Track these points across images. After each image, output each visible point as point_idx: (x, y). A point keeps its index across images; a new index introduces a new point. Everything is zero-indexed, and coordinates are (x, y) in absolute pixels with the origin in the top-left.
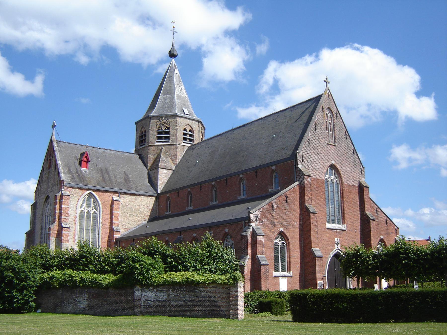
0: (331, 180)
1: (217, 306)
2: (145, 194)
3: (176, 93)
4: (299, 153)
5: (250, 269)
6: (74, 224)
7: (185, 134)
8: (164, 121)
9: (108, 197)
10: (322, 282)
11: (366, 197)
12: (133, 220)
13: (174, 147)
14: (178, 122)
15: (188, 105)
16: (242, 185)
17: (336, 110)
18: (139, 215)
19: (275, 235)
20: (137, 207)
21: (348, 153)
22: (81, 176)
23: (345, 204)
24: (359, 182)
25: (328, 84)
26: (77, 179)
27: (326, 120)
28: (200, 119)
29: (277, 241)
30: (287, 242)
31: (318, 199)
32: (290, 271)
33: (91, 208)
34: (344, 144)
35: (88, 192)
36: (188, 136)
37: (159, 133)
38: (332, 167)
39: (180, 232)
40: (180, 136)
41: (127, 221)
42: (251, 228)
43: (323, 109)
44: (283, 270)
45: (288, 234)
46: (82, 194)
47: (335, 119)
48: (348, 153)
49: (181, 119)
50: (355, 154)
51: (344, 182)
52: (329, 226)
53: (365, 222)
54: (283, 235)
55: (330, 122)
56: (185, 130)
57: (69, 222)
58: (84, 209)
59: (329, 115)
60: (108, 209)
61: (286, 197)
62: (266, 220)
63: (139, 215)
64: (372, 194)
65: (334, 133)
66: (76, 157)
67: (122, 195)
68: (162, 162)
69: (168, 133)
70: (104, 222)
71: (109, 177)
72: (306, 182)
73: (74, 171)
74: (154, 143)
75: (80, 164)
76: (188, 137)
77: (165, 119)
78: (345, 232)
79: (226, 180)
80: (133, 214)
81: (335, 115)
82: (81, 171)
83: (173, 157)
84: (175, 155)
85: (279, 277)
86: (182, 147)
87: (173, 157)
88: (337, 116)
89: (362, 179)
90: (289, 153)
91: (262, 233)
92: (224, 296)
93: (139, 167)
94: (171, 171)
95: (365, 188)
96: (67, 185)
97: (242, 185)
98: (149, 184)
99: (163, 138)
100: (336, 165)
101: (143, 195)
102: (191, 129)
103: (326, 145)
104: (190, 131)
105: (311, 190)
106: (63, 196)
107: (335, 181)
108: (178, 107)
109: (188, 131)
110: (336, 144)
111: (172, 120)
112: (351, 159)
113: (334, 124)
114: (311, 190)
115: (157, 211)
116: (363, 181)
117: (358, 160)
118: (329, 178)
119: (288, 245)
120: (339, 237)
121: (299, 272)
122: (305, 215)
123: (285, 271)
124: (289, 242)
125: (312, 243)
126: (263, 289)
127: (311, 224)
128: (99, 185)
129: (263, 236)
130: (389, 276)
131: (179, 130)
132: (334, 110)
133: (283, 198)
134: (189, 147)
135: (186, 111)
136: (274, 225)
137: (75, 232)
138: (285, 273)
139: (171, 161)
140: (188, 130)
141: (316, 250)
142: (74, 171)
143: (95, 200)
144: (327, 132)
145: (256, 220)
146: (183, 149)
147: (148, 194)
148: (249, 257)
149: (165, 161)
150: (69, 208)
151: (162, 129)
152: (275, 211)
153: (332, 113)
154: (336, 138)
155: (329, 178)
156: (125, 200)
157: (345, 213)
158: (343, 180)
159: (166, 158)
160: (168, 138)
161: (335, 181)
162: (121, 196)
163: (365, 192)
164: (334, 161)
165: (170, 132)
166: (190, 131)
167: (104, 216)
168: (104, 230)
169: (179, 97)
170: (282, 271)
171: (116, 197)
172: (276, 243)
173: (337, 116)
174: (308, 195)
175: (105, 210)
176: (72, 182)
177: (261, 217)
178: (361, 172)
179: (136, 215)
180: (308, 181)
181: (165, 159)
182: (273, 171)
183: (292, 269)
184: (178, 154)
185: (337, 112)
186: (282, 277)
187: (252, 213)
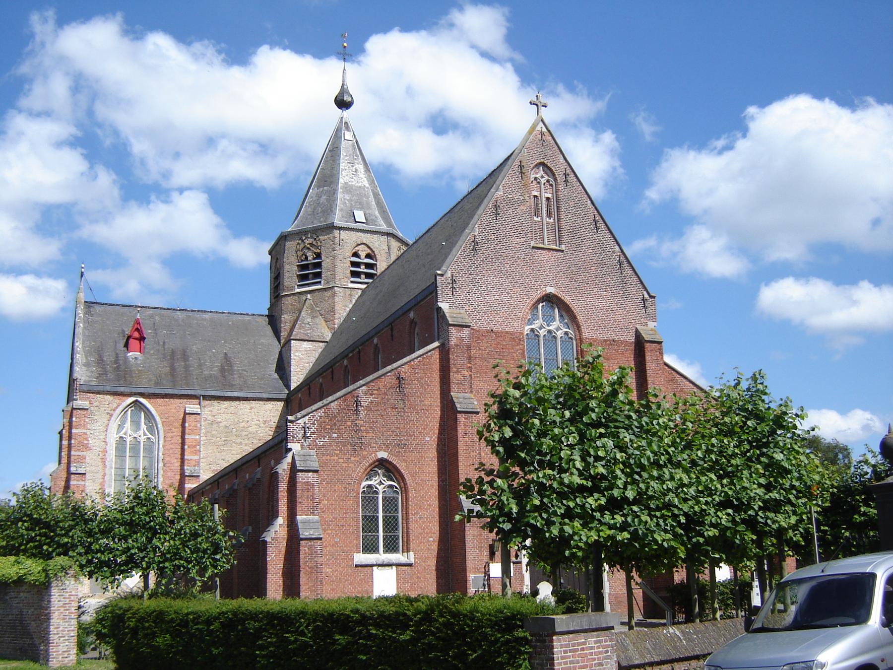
0: (550, 332)
2: (259, 395)
3: (341, 180)
4: (442, 275)
5: (284, 550)
6: (101, 466)
7: (354, 264)
8: (311, 240)
9: (176, 407)
12: (233, 452)
13: (328, 294)
14: (337, 240)
15: (368, 204)
19: (361, 469)
21: (602, 264)
22: (123, 367)
24: (637, 331)
26: (111, 376)
27: (537, 194)
30: (402, 484)
32: (408, 551)
33: (141, 432)
35: (132, 399)
36: (363, 267)
37: (303, 267)
38: (551, 300)
40: (343, 268)
42: (290, 455)
44: (391, 547)
46: (119, 405)
47: (561, 187)
48: (602, 264)
49: (344, 234)
51: (586, 334)
54: (390, 467)
55: (550, 196)
56: (356, 255)
57: (88, 460)
58: (125, 434)
59: (543, 181)
60: (178, 432)
63: (246, 442)
66: (123, 331)
67: (207, 402)
68: (301, 327)
69: (319, 265)
70: (167, 459)
71: (187, 367)
73: (109, 358)
74: (293, 288)
75: (126, 345)
76: (362, 269)
77: (312, 237)
79: (359, 352)
80: (233, 439)
81: (560, 178)
82: (126, 359)
84: (332, 311)
85: (372, 566)
87: (329, 315)
88: (566, 181)
91: (315, 465)
93: (263, 341)
94: (321, 344)
95: (647, 345)
96: (85, 388)
98: (276, 376)
99: (311, 276)
101: (254, 399)
102: (369, 251)
103: (529, 250)
104: (368, 256)
105: (470, 358)
106: (75, 412)
107: (559, 334)
108: (341, 210)
110: (563, 247)
111: (326, 237)
114: (470, 358)
116: (649, 329)
117: (635, 279)
118: (541, 327)
119: (405, 490)
121: (435, 553)
123: (375, 550)
124: (405, 484)
127: (460, 439)
128: (158, 384)
129: (316, 471)
130: (617, 559)
132: (559, 168)
133: (390, 380)
134: (363, 291)
135: (360, 216)
136: (358, 446)
137: (104, 481)
138: (382, 556)
139: (324, 323)
140: (363, 254)
142: (109, 358)
143: (149, 416)
144: (539, 219)
145: (305, 437)
146: (351, 295)
147: (265, 396)
148: (281, 521)
150: (86, 434)
151: (306, 258)
152: (363, 413)
153: (554, 175)
154: (564, 233)
155: (541, 327)
156: (212, 411)
158: (584, 329)
159: (314, 317)
160: (318, 275)
161: (559, 334)
162: (204, 403)
164: (556, 286)
166: (368, 256)
167: (168, 446)
168: (169, 474)
169: (348, 189)
170: (386, 552)
171: (192, 407)
172: (370, 486)
173: (566, 181)
175: (170, 435)
176: (99, 382)
178: (645, 307)
179: (239, 440)
180: (462, 339)
181: (309, 320)
183: (412, 545)
184: (337, 308)
185: (569, 171)
186: (379, 565)
187: (292, 422)
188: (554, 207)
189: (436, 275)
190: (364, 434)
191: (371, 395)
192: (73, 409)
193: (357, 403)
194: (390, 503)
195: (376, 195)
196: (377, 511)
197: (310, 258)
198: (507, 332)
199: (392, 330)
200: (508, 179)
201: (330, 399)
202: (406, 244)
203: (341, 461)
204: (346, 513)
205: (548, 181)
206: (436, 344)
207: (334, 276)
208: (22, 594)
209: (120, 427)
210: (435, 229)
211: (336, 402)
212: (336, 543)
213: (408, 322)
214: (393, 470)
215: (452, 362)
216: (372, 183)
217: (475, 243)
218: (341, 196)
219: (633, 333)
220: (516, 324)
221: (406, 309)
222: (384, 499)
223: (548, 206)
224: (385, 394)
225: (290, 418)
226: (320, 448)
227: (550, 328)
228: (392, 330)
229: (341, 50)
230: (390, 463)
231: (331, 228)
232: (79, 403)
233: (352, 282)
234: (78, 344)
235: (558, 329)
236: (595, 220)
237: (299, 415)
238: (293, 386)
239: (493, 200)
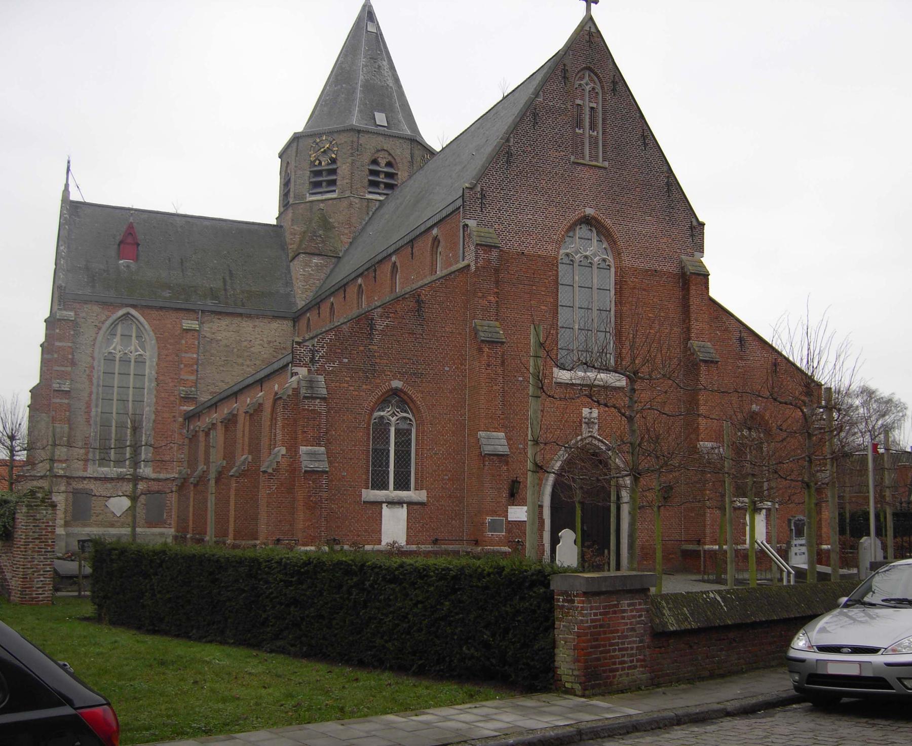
7: (373, 173)
11: (694, 301)
12: (234, 373)
18: (248, 362)
20: (245, 343)
36: (382, 176)
38: (587, 221)
46: (108, 317)
54: (405, 397)
56: (375, 162)
58: (115, 349)
59: (588, 88)
61: (419, 302)
63: (248, 362)
69: (333, 172)
70: (161, 378)
76: (381, 178)
85: (381, 503)
99: (324, 184)
104: (389, 164)
118: (577, 252)
123: (408, 488)
126: (526, 519)
137: (90, 400)
138: (392, 493)
140: (383, 162)
151: (320, 163)
152: (377, 338)
160: (333, 183)
164: (596, 207)
165: (338, 171)
166: (389, 164)
168: (163, 395)
170: (416, 489)
172: (382, 417)
182: (436, 240)
190: (378, 361)
191: (388, 318)
193: (372, 327)
197: (323, 163)
198: (539, 256)
203: (352, 388)
204: (355, 446)
212: (343, 477)
214: (409, 401)
220: (550, 248)
226: (329, 373)
230: (405, 393)
233: (370, 192)
235: (595, 255)
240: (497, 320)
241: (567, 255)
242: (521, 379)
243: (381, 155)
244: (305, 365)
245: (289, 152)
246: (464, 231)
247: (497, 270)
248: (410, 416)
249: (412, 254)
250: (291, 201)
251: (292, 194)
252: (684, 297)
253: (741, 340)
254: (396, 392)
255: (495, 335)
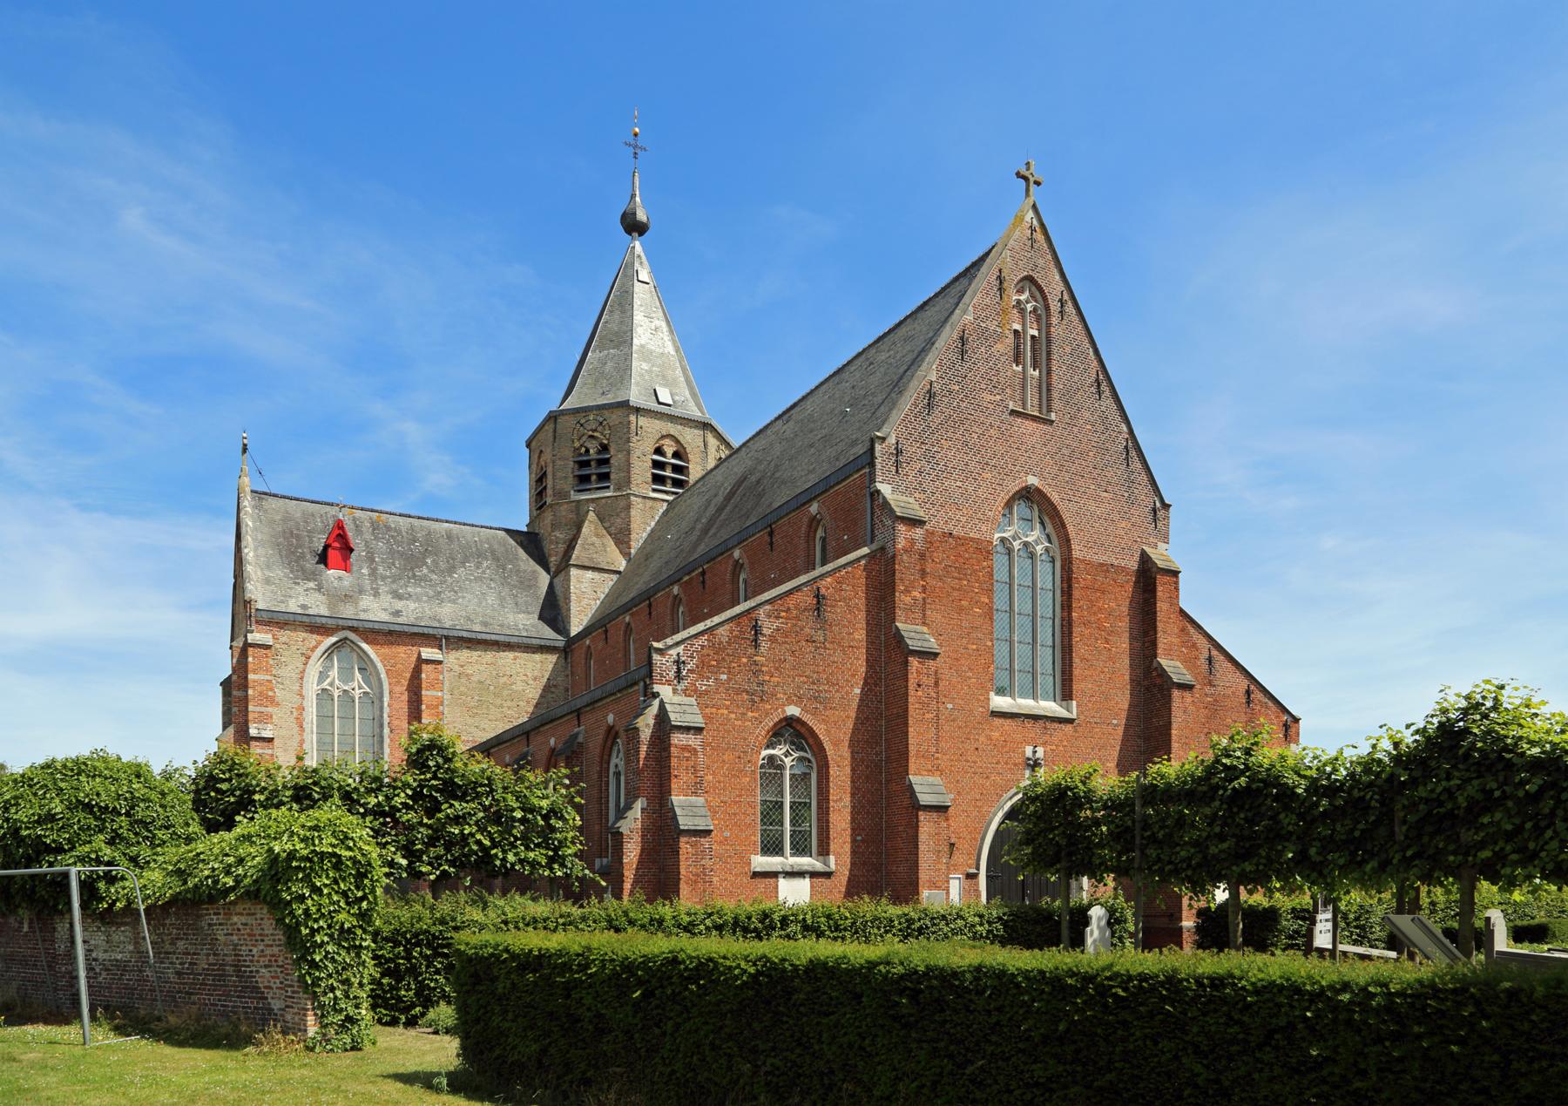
0: (1026, 544)
1: (256, 989)
7: (656, 464)
10: (954, 887)
11: (1162, 606)
14: (633, 427)
15: (675, 380)
16: (742, 586)
17: (1061, 287)
20: (502, 680)
23: (1076, 630)
24: (1144, 554)
25: (1033, 187)
27: (1017, 327)
28: (708, 417)
29: (778, 751)
31: (961, 610)
34: (1087, 415)
36: (669, 469)
38: (1028, 495)
39: (527, 734)
40: (641, 470)
41: (470, 721)
42: (656, 702)
43: (1000, 279)
44: (800, 849)
45: (819, 729)
46: (319, 643)
47: (1055, 320)
49: (643, 421)
50: (1133, 453)
51: (1076, 554)
52: (1000, 702)
53: (1152, 694)
54: (803, 730)
55: (1036, 333)
56: (659, 451)
58: (331, 684)
59: (1029, 307)
62: (724, 677)
64: (1193, 596)
65: (1049, 372)
69: (606, 462)
72: (901, 543)
76: (668, 473)
78: (1068, 728)
79: (703, 573)
81: (1055, 306)
83: (622, 539)
86: (650, 503)
89: (1156, 547)
90: (860, 449)
91: (698, 721)
92: (276, 950)
96: (265, 616)
97: (742, 586)
100: (1046, 490)
103: (1006, 416)
104: (676, 455)
106: (250, 650)
109: (669, 454)
110: (1053, 416)
112: (1116, 472)
113: (1049, 342)
115: (567, 690)
116: (1162, 554)
120: (1044, 744)
122: (889, 657)
125: (912, 760)
127: (911, 692)
131: (638, 453)
132: (1054, 288)
133: (805, 598)
138: (805, 862)
140: (669, 451)
141: (926, 786)
144: (1020, 368)
149: (594, 540)
151: (587, 451)
152: (764, 645)
153: (1045, 298)
154: (1055, 394)
157: (1076, 660)
160: (605, 477)
161: (1039, 549)
163: (1159, 588)
169: (647, 355)
171: (428, 653)
172: (771, 758)
174: (907, 591)
177: (703, 664)
179: (499, 702)
180: (912, 542)
182: (814, 522)
183: (832, 847)
185: (1066, 297)
188: (1042, 351)
189: (872, 442)
191: (777, 618)
192: (246, 645)
193: (757, 629)
194: (800, 780)
195: (684, 370)
196: (781, 793)
198: (972, 539)
199: (771, 534)
200: (980, 293)
201: (716, 619)
202: (728, 445)
205: (1035, 309)
206: (865, 550)
207: (628, 482)
208: (235, 919)
209: (323, 676)
210: (816, 398)
211: (727, 627)
213: (805, 520)
214: (807, 734)
215: (898, 575)
216: (677, 351)
217: (931, 394)
218: (638, 365)
219: (1137, 557)
220: (984, 528)
221: (803, 499)
222: (793, 776)
223: (1034, 350)
224: (797, 618)
225: (656, 645)
227: (1029, 539)
228: (771, 534)
229: (631, 139)
230: (804, 724)
231: (625, 405)
232: (256, 636)
233: (654, 490)
234: (249, 553)
235: (1037, 542)
236: (1097, 380)
237: (669, 641)
238: (574, 631)
239: (959, 327)
240: (924, 624)
241: (1003, 540)
242: (950, 706)
243: (667, 442)
244: (669, 683)
245: (541, 436)
246: (872, 500)
247: (922, 556)
248: (809, 756)
249: (771, 544)
250: (549, 500)
251: (549, 491)
252: (1145, 600)
253: (1210, 660)
254: (790, 722)
255: (926, 644)
